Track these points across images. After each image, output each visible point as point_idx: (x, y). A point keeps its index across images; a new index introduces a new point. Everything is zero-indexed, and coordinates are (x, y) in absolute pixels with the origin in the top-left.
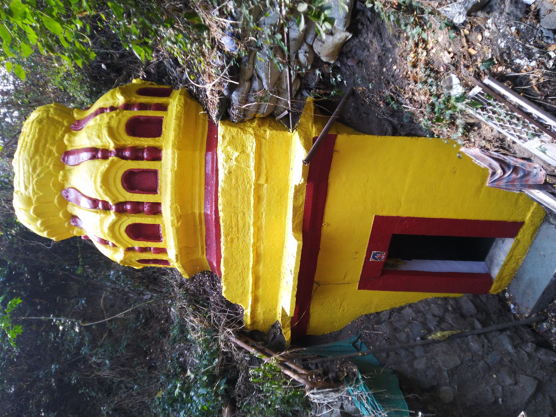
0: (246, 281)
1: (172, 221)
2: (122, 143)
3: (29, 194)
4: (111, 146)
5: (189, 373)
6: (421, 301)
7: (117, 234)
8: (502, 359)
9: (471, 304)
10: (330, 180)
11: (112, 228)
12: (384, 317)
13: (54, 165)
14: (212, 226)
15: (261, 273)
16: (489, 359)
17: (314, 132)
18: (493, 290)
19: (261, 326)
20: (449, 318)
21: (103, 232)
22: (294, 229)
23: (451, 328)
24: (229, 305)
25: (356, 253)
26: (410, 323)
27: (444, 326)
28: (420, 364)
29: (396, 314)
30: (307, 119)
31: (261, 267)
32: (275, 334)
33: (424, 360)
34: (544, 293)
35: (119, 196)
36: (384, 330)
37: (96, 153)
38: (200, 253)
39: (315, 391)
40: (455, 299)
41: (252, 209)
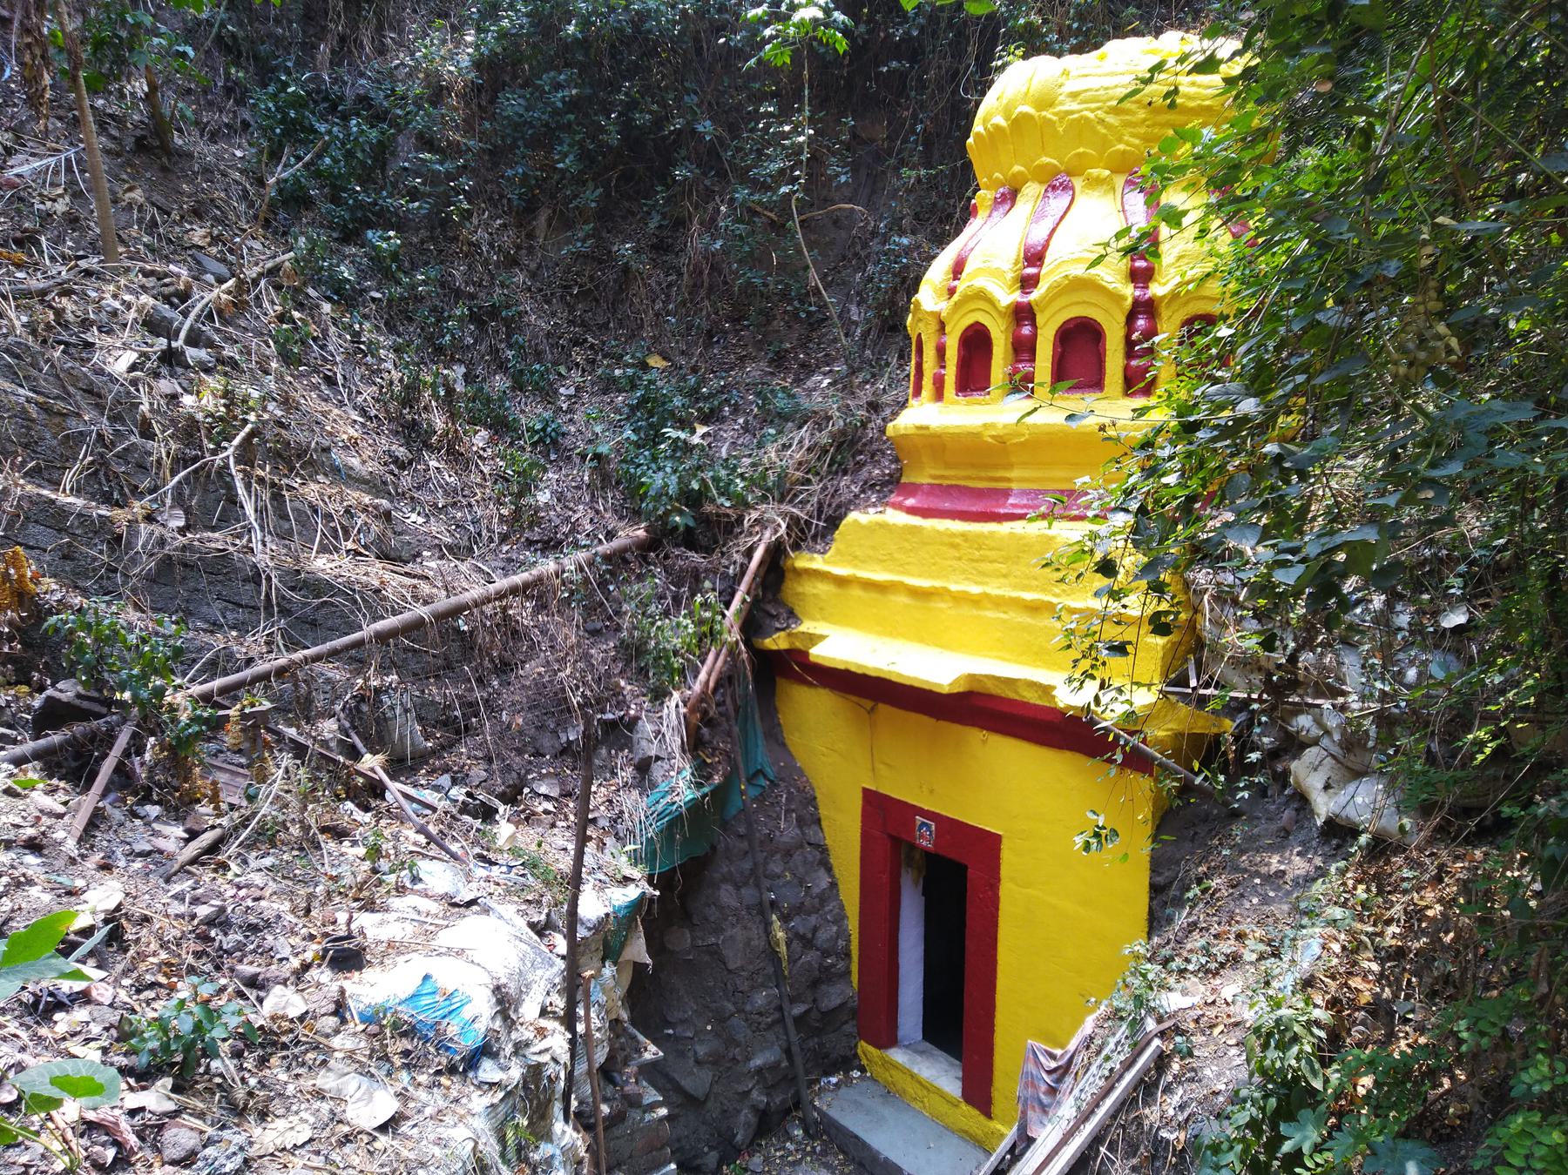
1: (993, 426)
2: (1165, 313)
3: (1061, 104)
4: (1157, 289)
6: (842, 907)
7: (973, 306)
8: (738, 1045)
9: (839, 1001)
10: (1068, 754)
11: (982, 296)
12: (811, 832)
13: (1124, 152)
15: (892, 598)
16: (737, 1021)
18: (864, 1047)
19: (797, 590)
20: (810, 957)
22: (972, 678)
23: (792, 960)
24: (834, 522)
25: (932, 791)
26: (801, 882)
27: (796, 945)
28: (727, 895)
29: (818, 856)
30: (1182, 719)
31: (903, 599)
32: (776, 617)
33: (734, 903)
34: (856, 1137)
35: (1047, 314)
36: (787, 831)
37: (1141, 256)
38: (933, 472)
39: (683, 710)
40: (850, 973)
41: (1014, 594)
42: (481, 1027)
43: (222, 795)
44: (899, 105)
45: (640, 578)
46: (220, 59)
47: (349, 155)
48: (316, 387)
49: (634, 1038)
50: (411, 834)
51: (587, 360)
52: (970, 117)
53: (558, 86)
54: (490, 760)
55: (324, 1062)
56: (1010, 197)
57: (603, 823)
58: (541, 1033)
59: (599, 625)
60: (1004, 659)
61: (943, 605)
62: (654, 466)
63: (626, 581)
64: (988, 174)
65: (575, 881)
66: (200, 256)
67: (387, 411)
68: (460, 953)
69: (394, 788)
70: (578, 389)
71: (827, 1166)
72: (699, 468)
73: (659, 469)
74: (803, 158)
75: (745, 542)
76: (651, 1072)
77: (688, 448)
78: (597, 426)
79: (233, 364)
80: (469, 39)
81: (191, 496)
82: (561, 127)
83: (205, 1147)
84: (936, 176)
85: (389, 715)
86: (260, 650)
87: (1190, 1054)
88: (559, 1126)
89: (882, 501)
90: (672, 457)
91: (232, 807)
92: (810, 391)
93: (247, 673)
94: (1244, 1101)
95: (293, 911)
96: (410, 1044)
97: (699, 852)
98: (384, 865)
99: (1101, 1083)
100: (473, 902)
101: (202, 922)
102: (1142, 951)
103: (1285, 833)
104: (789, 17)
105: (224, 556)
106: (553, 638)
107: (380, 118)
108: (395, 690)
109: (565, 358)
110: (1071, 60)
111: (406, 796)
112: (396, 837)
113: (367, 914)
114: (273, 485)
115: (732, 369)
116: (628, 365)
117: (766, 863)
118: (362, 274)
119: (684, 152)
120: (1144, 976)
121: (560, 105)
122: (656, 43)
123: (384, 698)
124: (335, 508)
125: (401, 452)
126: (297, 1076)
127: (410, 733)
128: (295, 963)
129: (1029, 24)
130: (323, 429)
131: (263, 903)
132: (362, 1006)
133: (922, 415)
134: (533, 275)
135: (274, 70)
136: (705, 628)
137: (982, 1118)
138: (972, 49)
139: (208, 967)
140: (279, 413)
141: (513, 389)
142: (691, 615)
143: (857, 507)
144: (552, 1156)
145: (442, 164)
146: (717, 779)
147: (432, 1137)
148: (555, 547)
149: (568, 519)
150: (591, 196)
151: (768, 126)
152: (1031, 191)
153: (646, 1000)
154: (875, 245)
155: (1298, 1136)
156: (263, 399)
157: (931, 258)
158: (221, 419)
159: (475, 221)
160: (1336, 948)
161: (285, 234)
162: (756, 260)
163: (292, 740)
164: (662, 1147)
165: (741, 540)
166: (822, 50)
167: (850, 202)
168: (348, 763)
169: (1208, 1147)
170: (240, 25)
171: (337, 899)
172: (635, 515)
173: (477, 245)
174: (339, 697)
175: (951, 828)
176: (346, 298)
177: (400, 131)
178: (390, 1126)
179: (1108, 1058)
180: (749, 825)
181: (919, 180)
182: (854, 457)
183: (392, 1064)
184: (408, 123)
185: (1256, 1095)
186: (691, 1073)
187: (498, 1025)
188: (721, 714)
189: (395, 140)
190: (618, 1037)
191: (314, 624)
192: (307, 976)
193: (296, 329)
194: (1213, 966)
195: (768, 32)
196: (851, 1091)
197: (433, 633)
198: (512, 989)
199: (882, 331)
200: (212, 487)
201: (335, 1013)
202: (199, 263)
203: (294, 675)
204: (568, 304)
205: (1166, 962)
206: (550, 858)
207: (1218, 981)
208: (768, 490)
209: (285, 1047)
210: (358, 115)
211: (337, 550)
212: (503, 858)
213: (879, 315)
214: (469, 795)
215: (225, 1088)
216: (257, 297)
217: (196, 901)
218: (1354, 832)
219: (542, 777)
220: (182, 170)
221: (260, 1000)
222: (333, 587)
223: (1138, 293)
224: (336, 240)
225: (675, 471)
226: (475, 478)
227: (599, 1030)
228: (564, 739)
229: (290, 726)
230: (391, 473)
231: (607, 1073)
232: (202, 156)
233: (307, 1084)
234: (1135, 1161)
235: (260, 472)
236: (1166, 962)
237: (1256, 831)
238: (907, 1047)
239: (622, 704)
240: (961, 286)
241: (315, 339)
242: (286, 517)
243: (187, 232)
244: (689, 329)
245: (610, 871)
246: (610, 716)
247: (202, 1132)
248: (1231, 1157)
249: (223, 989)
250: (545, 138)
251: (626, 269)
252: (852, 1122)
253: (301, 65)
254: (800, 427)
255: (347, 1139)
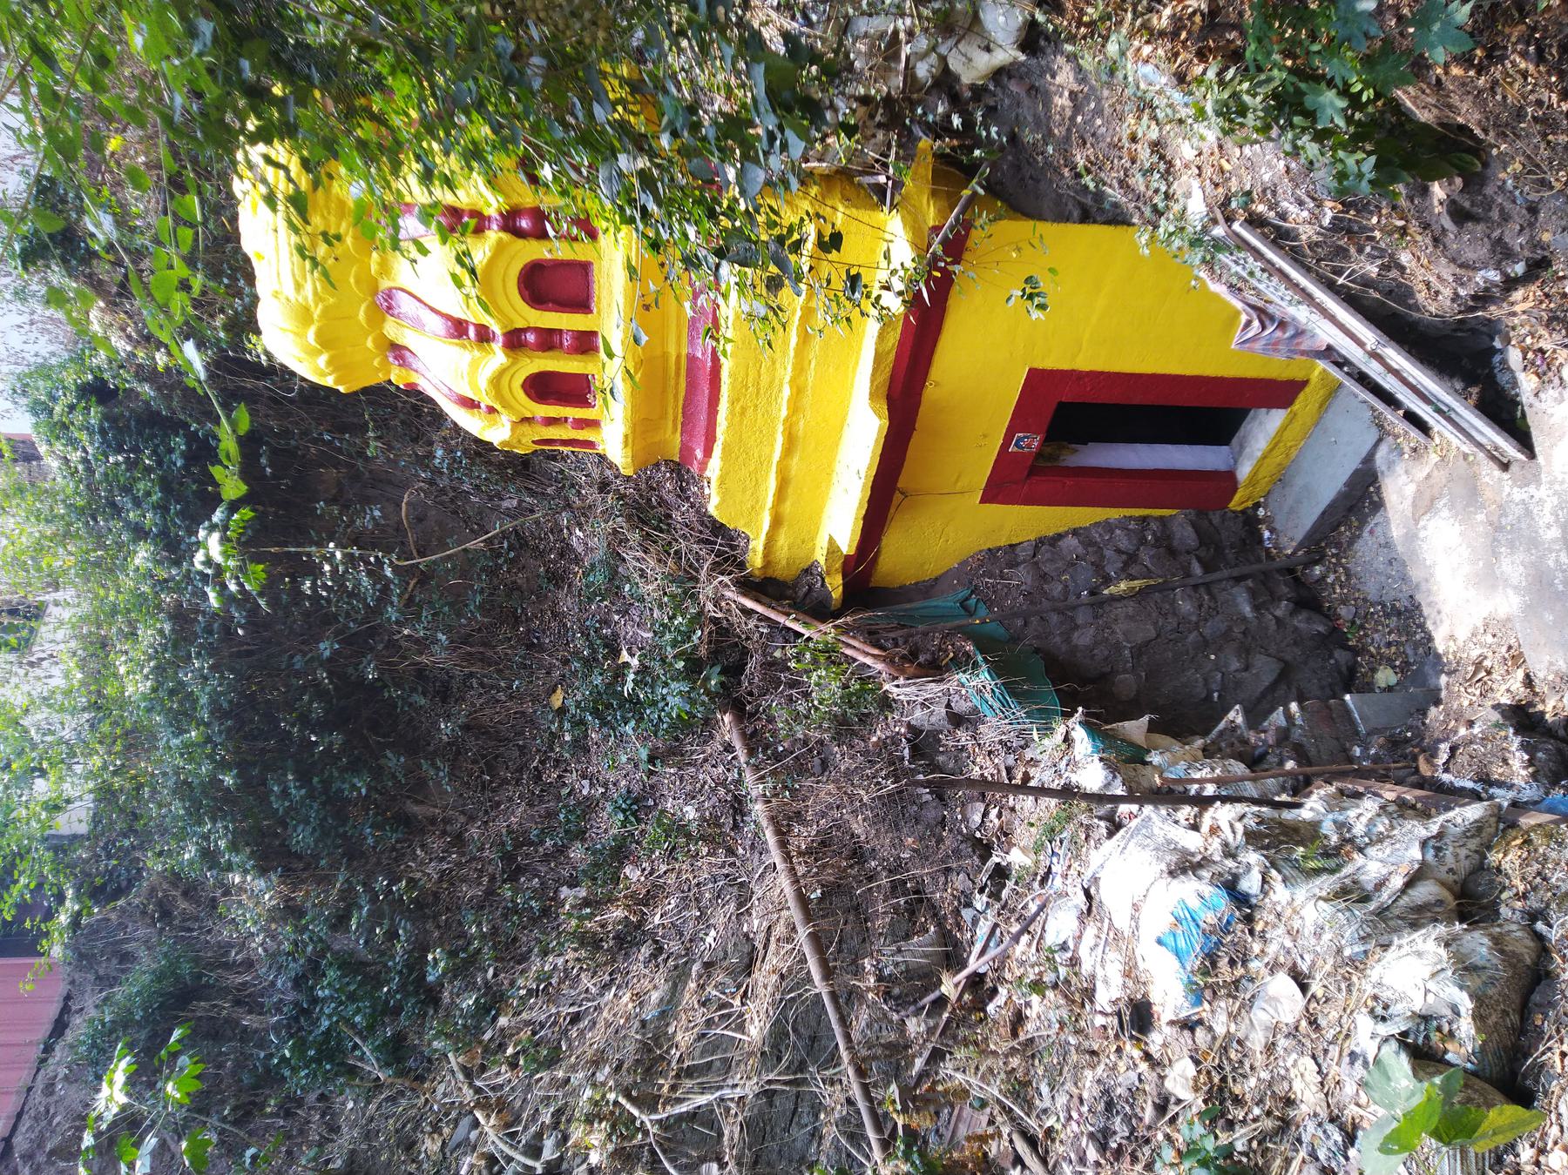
0: (763, 487)
2: (516, 200)
3: (306, 299)
5: (625, 656)
6: (1097, 524)
8: (1230, 629)
10: (951, 302)
11: (496, 381)
12: (1022, 555)
14: (702, 380)
15: (793, 473)
16: (1207, 631)
17: (931, 216)
18: (1236, 503)
19: (782, 571)
20: (1145, 556)
21: (472, 384)
22: (873, 396)
23: (1148, 574)
24: (718, 528)
27: (1133, 570)
28: (1083, 638)
30: (916, 183)
31: (795, 462)
32: (811, 586)
33: (1092, 631)
34: (1323, 513)
39: (901, 681)
40: (1161, 519)
41: (792, 354)
42: (1208, 890)
43: (979, 1131)
44: (304, 456)
45: (771, 720)
46: (258, 1122)
47: (352, 997)
48: (582, 1033)
49: (1221, 733)
50: (1020, 949)
51: (555, 767)
52: (315, 387)
53: (285, 793)
54: (948, 870)
55: (1239, 1042)
56: (398, 352)
57: (1011, 760)
58: (1214, 830)
59: (817, 761)
60: (857, 363)
61: (802, 423)
62: (661, 705)
63: (774, 733)
64: (375, 372)
65: (1068, 793)
66: (451, 1144)
67: (606, 964)
68: (1136, 907)
69: (974, 964)
70: (584, 777)
71: (1352, 541)
72: (663, 660)
73: (664, 699)
74: (357, 554)
75: (736, 618)
76: (1255, 716)
77: (643, 670)
78: (621, 759)
79: (558, 1113)
80: (237, 880)
81: (688, 1156)
82: (326, 790)
83: (1317, 1159)
84: (375, 421)
85: (903, 968)
86: (840, 1089)
87: (1249, 193)
88: (1305, 814)
89: (699, 480)
90: (652, 687)
91: (991, 1122)
92: (588, 549)
93: (862, 1105)
94: (1295, 147)
95: (1093, 1068)
96: (1221, 963)
97: (1041, 666)
98: (1049, 977)
99: (1275, 280)
100: (1087, 893)
101: (1103, 1155)
102: (1146, 236)
103: (1033, 90)
104: (218, 565)
105: (747, 1125)
106: (830, 807)
107: (314, 968)
108: (878, 961)
109: (553, 789)
110: (262, 287)
111: (983, 952)
112: (1022, 963)
113: (1097, 996)
114: (678, 1076)
115: (565, 625)
116: (561, 727)
117: (1052, 599)
118: (471, 986)
119: (350, 670)
120: (1171, 235)
121: (303, 792)
122: (241, 694)
123: (887, 972)
124: (700, 1016)
125: (645, 951)
126: (1252, 1068)
127: (920, 948)
128: (1143, 1067)
129: (226, 328)
130: (623, 1027)
131: (1085, 1095)
132: (1186, 1004)
133: (614, 438)
134: (472, 819)
135: (268, 1070)
136: (822, 660)
137: (1307, 390)
138: (249, 383)
139: (1147, 1150)
140: (607, 1069)
141: (583, 840)
142: (808, 672)
143: (703, 506)
144: (1335, 822)
145: (361, 908)
146: (969, 647)
147: (1313, 941)
148: (740, 802)
149: (713, 790)
150: (394, 761)
151: (325, 587)
152: (391, 330)
153: (1184, 720)
154: (443, 482)
155: (1329, 111)
156: (594, 1085)
157: (456, 428)
158: (613, 1127)
159: (418, 875)
160: (1147, 50)
161: (430, 1061)
162: (457, 601)
163: (928, 1063)
164: (1328, 707)
165: (735, 620)
166: (250, 532)
167: (399, 506)
168: (949, 1008)
169: (1340, 183)
170: (223, 1102)
171: (1083, 1023)
172: (709, 723)
173: (442, 873)
174: (885, 1015)
175: (1021, 418)
176: (493, 1001)
177: (329, 948)
178: (1301, 981)
179: (1251, 274)
180: (1016, 615)
181: (377, 438)
182: (653, 508)
183: (1242, 977)
184: (321, 940)
185: (1290, 135)
186: (1257, 675)
187: (1206, 874)
188: (906, 642)
189: (337, 953)
190: (1220, 750)
191: (813, 1039)
192: (1156, 1056)
193: (524, 1051)
194: (1162, 166)
195: (233, 587)
196: (1278, 518)
197: (824, 924)
198: (1173, 858)
199: (528, 477)
200: (680, 1136)
201: (1192, 1030)
202: (458, 1146)
203: (864, 1060)
204: (500, 785)
205: (1158, 213)
206: (1045, 815)
207: (1178, 163)
208: (685, 593)
209: (1224, 1079)
210: (312, 988)
211: (741, 1015)
212: (1044, 860)
213: (512, 479)
214: (982, 891)
215: (1263, 1138)
216: (493, 1089)
217: (1082, 1160)
218: (1032, 25)
219: (965, 819)
220: (366, 1160)
221: (1179, 1101)
222: (778, 1020)
223: (495, 227)
224: (436, 1011)
225: (666, 684)
226: (671, 879)
227: (1213, 770)
228: (929, 797)
229: (913, 1063)
230: (666, 961)
231: (1255, 761)
232: (353, 1140)
233: (1259, 1059)
234: (1352, 250)
235: (665, 1089)
236: (1158, 213)
237: (1030, 119)
238: (1236, 462)
239: (895, 740)
240: (486, 401)
241: (534, 1033)
242: (709, 1064)
243: (428, 1157)
244: (525, 667)
245: (1058, 755)
246: (906, 751)
247: (1304, 1161)
248: (1351, 161)
249: (1168, 1137)
250: (337, 806)
251: (466, 728)
252: (1308, 517)
253: (263, 1043)
254: (624, 560)
255: (1313, 1023)
